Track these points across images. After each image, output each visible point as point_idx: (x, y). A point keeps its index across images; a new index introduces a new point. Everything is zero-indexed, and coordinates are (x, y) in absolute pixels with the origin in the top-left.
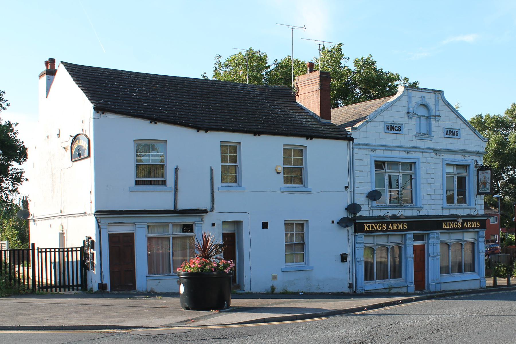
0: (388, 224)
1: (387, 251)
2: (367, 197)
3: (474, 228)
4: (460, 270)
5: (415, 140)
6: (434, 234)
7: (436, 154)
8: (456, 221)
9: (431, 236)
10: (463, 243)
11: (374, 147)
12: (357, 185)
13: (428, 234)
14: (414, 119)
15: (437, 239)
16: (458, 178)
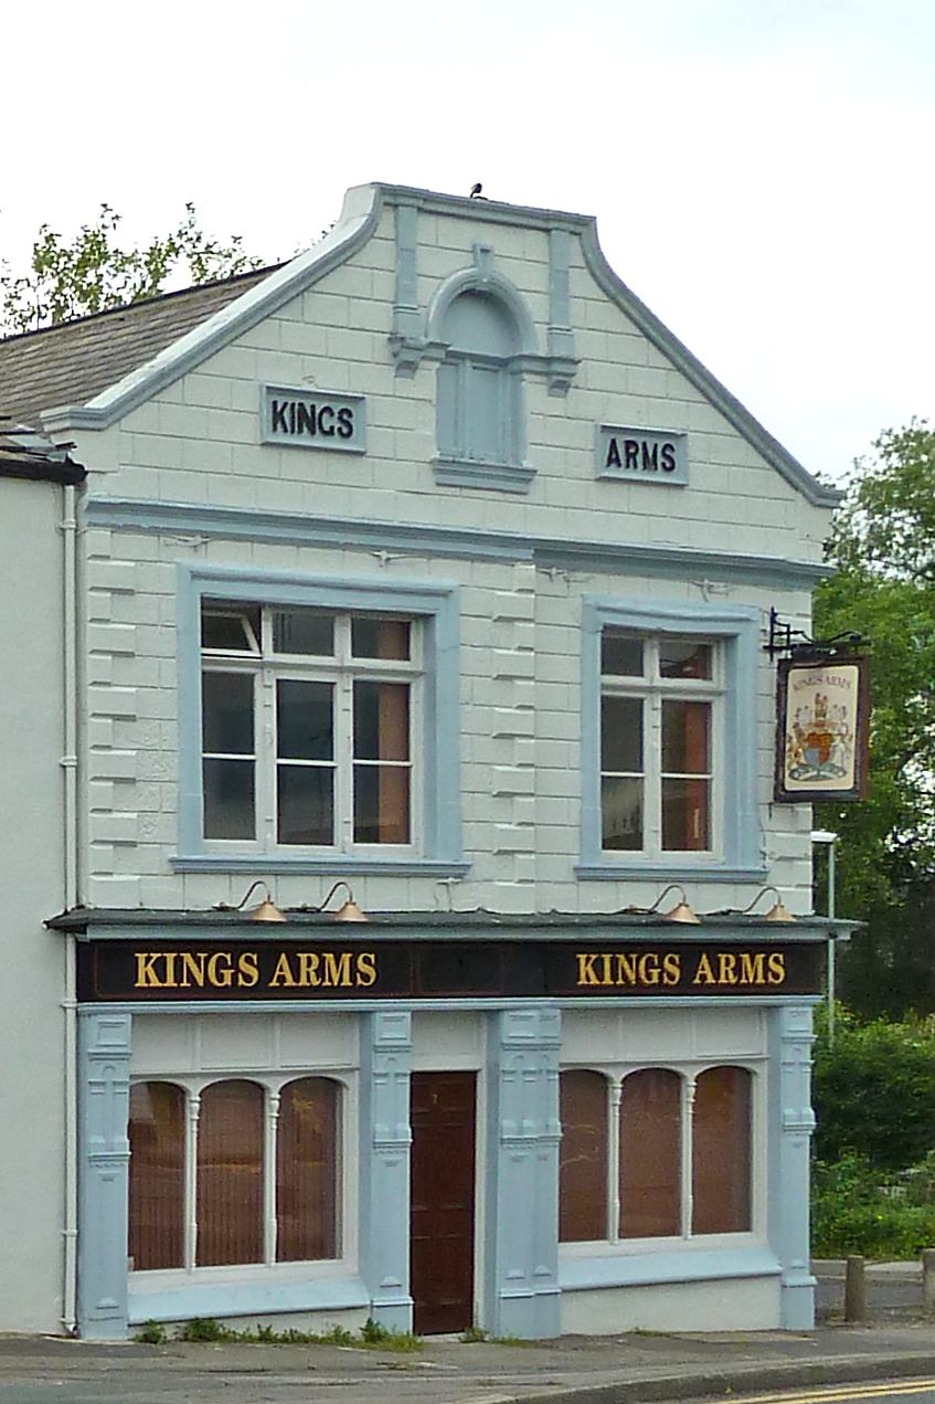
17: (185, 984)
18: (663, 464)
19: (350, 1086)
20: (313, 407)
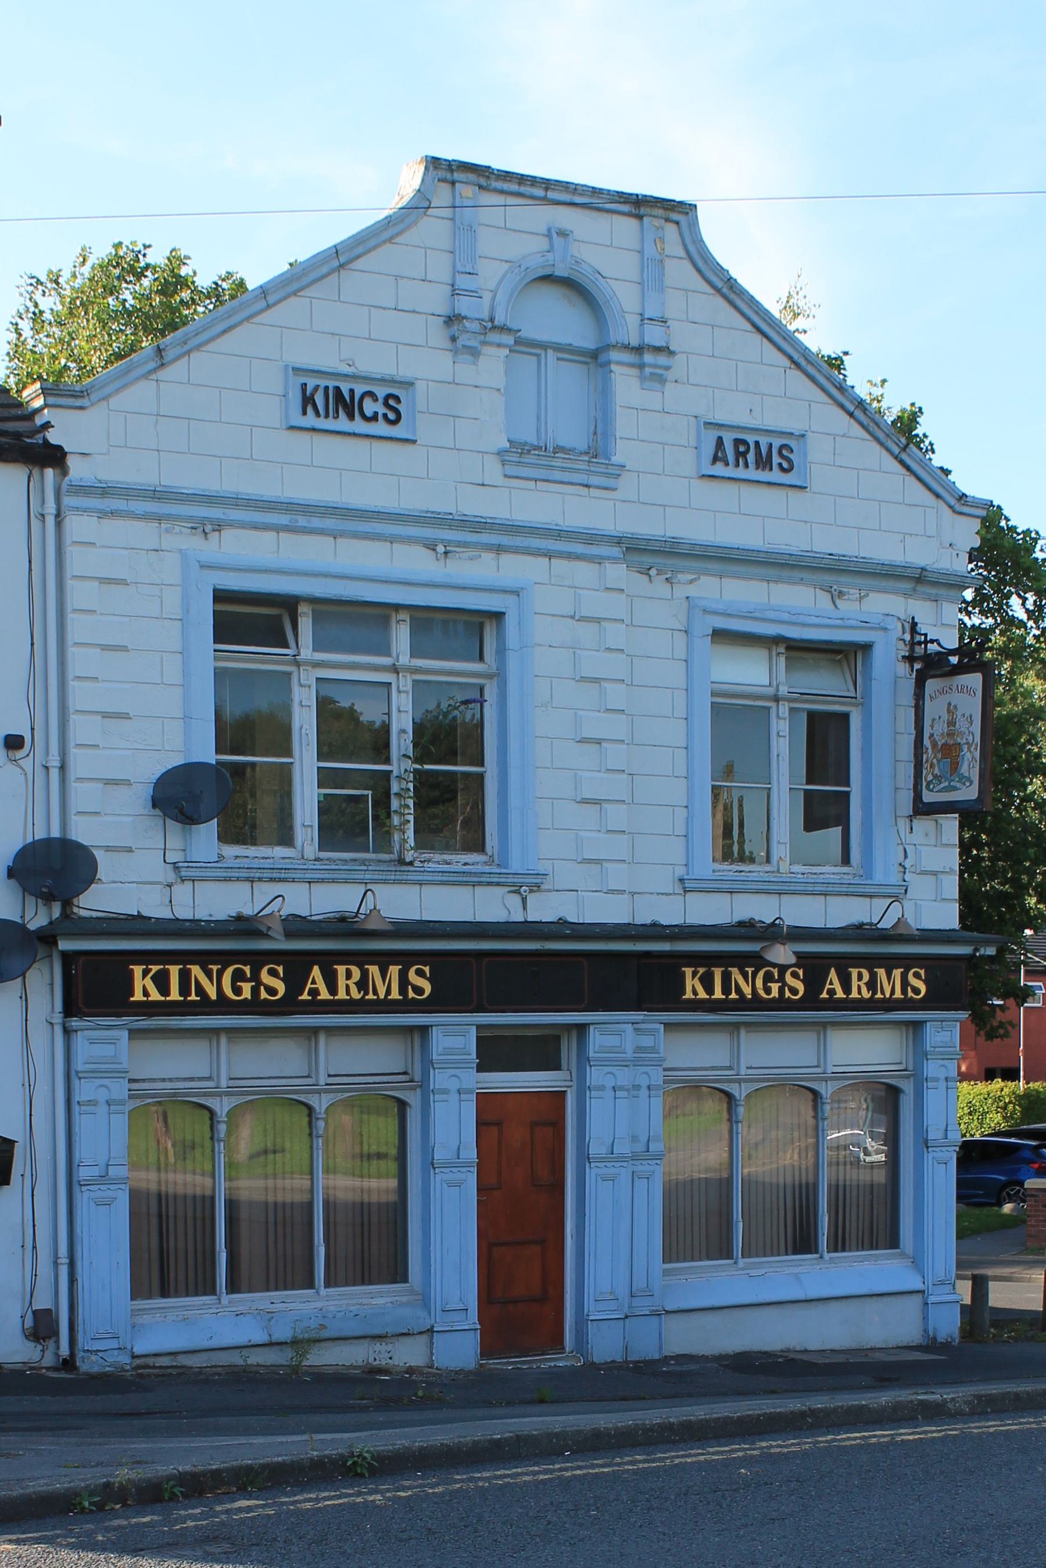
0: (296, 968)
1: (730, 1110)
2: (156, 802)
3: (889, 1005)
4: (803, 1242)
5: (500, 480)
6: (616, 1035)
7: (646, 572)
8: (757, 961)
9: (596, 1040)
10: (826, 1090)
11: (212, 513)
12: (81, 729)
13: (582, 1029)
14: (493, 364)
15: (637, 1062)
16: (815, 720)
17: (193, 997)
18: (780, 465)
19: (907, 1092)
20: (352, 391)
